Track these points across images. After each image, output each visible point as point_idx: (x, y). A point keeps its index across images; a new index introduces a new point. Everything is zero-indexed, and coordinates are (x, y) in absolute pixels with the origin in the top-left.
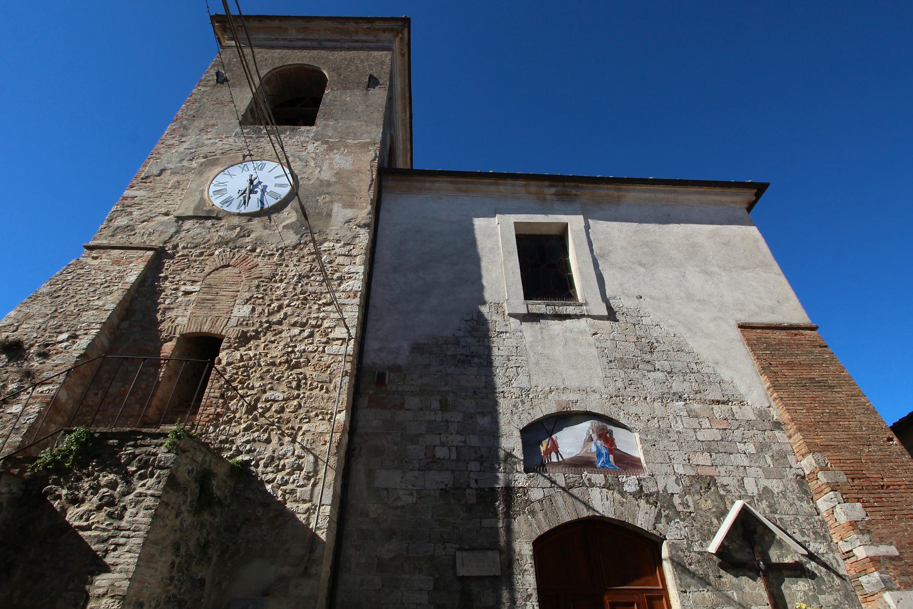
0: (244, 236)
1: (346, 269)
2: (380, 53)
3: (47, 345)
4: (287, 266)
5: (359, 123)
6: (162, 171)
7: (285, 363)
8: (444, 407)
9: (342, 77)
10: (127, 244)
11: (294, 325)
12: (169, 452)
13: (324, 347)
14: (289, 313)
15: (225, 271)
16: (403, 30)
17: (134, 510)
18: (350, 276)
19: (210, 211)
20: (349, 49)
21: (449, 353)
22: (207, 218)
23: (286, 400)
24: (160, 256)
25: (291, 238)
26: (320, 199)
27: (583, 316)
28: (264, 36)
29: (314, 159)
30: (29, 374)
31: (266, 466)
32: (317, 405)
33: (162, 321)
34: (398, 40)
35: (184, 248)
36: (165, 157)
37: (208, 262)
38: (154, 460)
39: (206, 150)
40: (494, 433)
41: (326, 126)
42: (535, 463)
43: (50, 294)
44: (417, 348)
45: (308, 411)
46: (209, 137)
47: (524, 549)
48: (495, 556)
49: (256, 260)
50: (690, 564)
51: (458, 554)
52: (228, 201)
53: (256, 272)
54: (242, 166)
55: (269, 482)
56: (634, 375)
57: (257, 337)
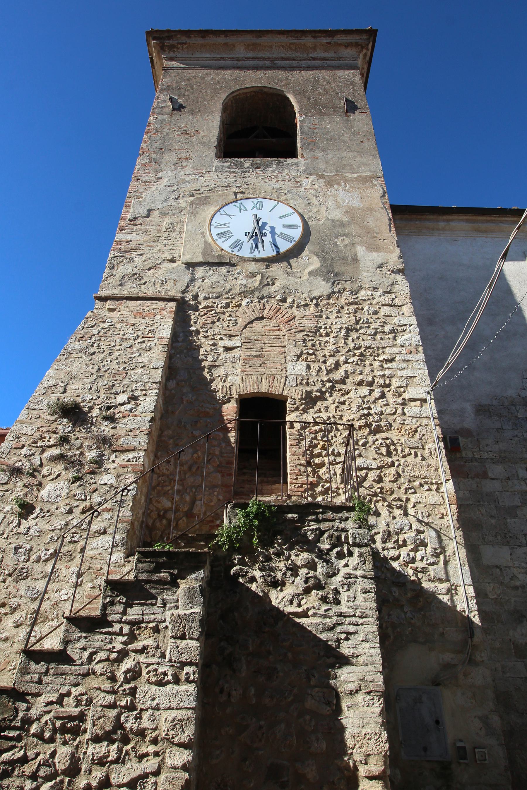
0: (268, 284)
1: (396, 321)
2: (347, 72)
3: (109, 408)
4: (328, 318)
5: (351, 154)
6: (150, 211)
7: (365, 426)
9: (312, 101)
10: (141, 295)
11: (360, 384)
12: (360, 527)
13: (403, 409)
14: (350, 371)
15: (261, 324)
16: (368, 45)
17: (350, 593)
18: (403, 328)
19: (220, 256)
20: (309, 68)
21: (520, 415)
22: (221, 264)
25: (322, 288)
26: (339, 241)
29: (315, 196)
30: (104, 441)
31: (384, 541)
32: (417, 473)
33: (212, 380)
34: (361, 56)
35: (206, 298)
36: (147, 196)
37: (238, 314)
38: (346, 537)
39: (188, 187)
41: (315, 158)
43: (84, 350)
44: (481, 410)
45: (410, 481)
46: (187, 172)
49: (290, 311)
52: (237, 245)
53: (296, 324)
54: (237, 204)
57: (322, 398)
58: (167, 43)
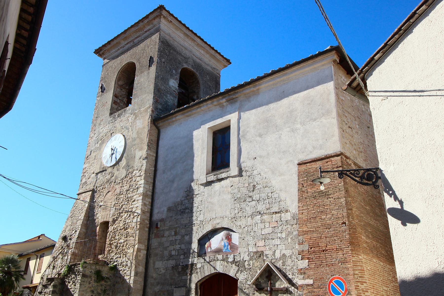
8: (176, 234)
15: (108, 194)
23: (124, 242)
24: (93, 191)
27: (228, 177)
28: (114, 50)
40: (190, 243)
42: (202, 253)
47: (193, 286)
48: (184, 289)
50: (245, 289)
51: (174, 289)
55: (121, 270)
56: (243, 205)
57: (117, 220)
58: (101, 52)
